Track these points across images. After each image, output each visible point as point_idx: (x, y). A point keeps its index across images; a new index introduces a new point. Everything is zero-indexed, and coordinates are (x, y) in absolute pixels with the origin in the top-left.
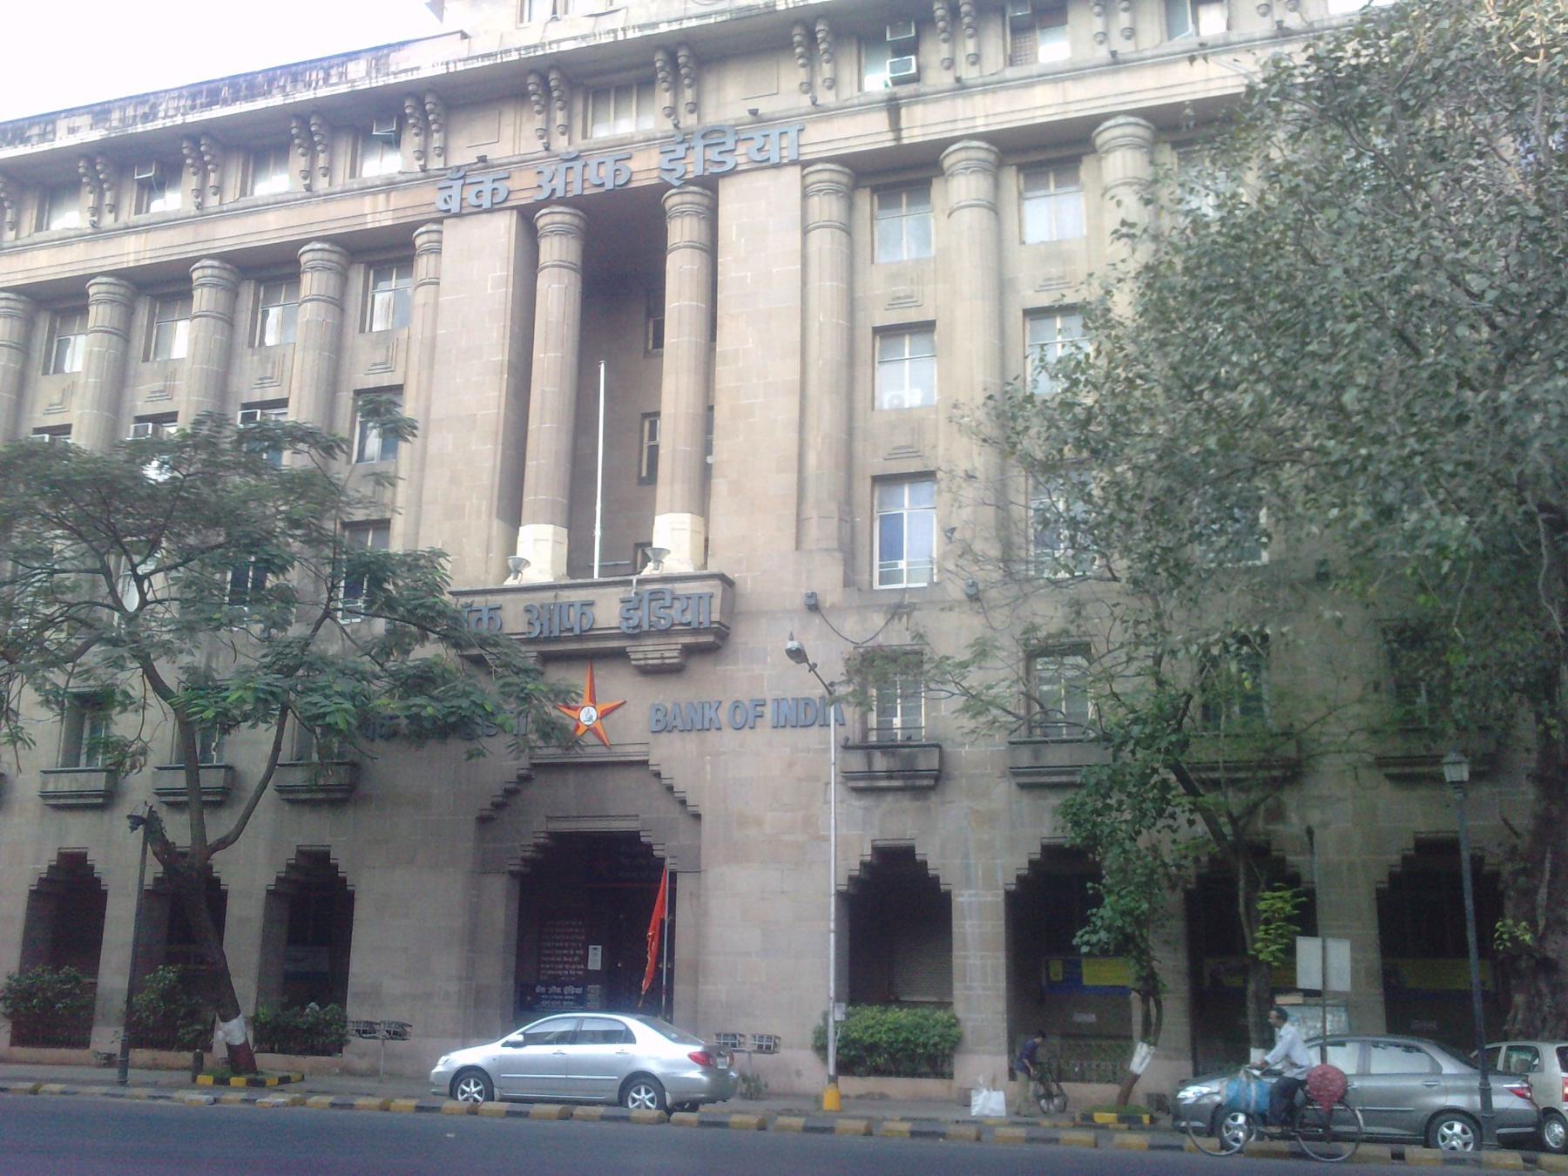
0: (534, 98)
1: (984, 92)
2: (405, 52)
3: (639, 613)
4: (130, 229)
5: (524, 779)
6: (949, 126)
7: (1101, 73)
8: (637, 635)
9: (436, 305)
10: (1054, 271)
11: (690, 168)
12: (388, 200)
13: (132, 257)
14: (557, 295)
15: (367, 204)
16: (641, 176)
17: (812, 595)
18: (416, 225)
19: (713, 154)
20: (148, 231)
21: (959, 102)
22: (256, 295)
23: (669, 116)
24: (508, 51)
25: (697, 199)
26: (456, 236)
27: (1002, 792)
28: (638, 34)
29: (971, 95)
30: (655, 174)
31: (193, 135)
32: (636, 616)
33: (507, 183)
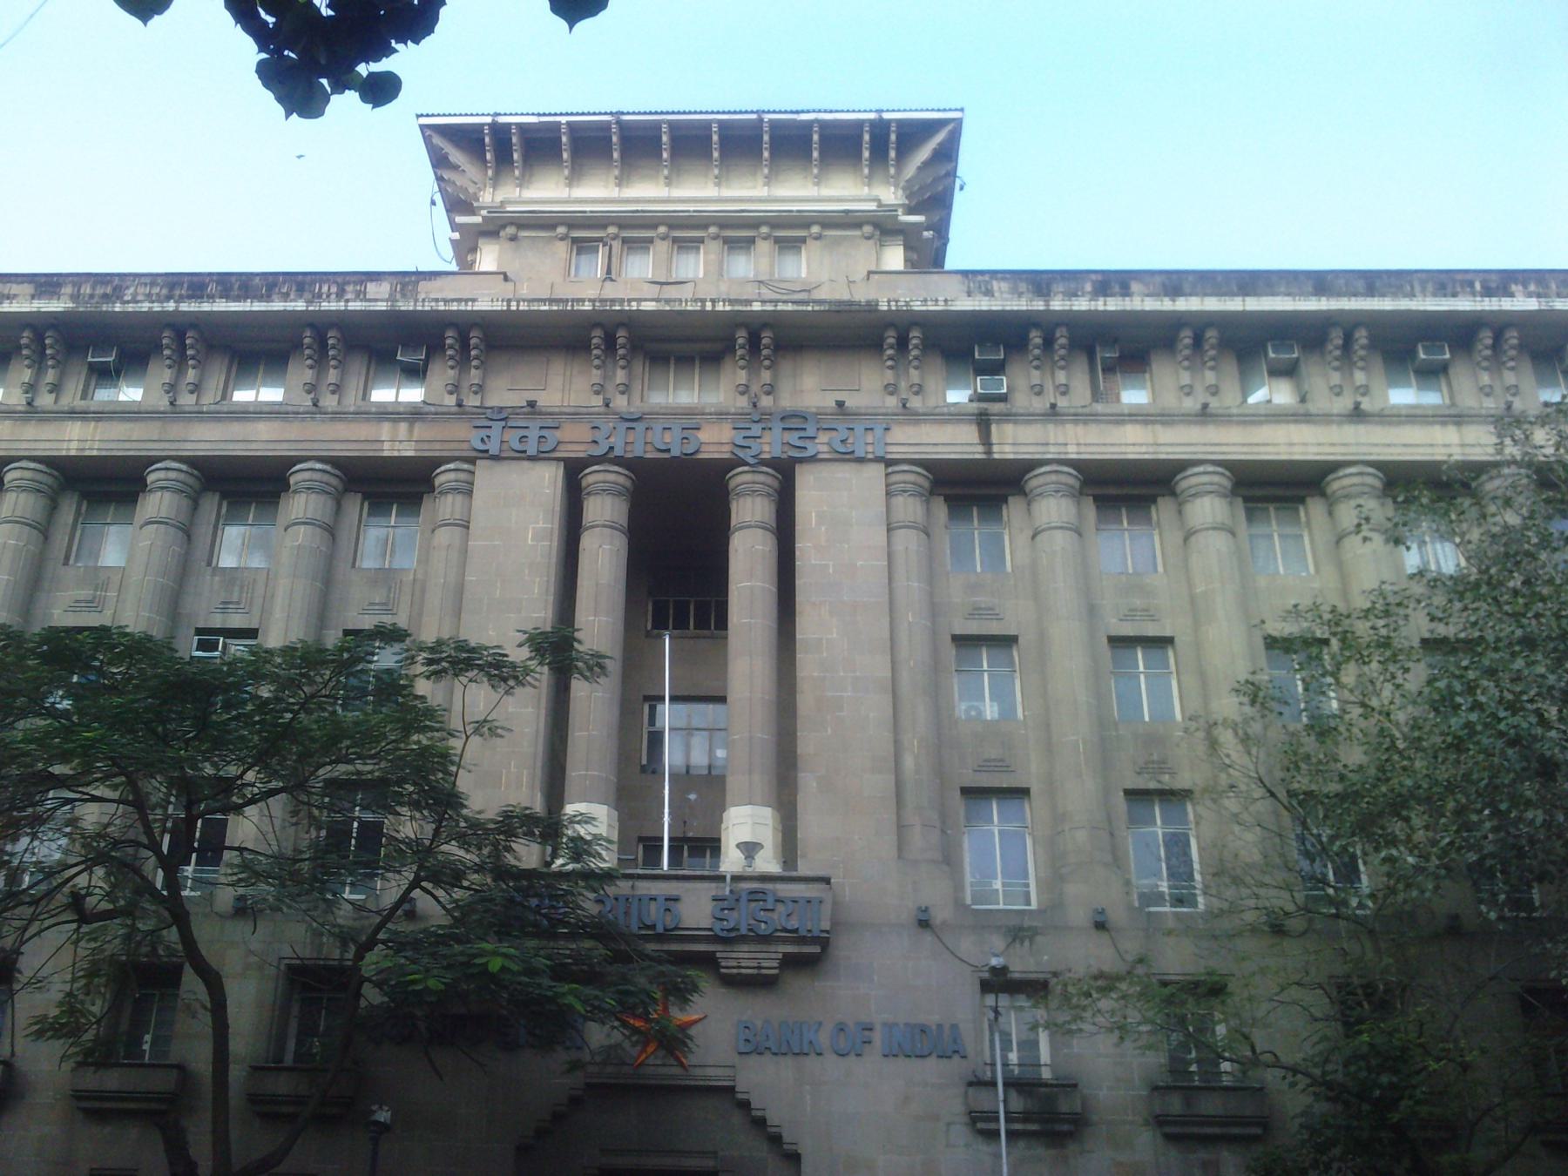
0: (450, 352)
1: (1076, 422)
2: (439, 282)
3: (735, 914)
4: (73, 414)
5: (575, 1101)
6: (1041, 449)
7: (1190, 423)
8: (731, 939)
9: (464, 551)
10: (1138, 602)
11: (766, 448)
12: (411, 431)
13: (74, 445)
14: (604, 557)
15: (385, 431)
16: (711, 448)
18: (437, 462)
19: (793, 438)
20: (99, 420)
21: (1051, 427)
22: (78, 513)
23: (309, 392)
24: (583, 300)
25: (769, 480)
26: (488, 478)
27: (1146, 1145)
28: (728, 308)
29: (1063, 422)
30: (727, 448)
31: (180, 327)
32: (733, 918)
33: (558, 434)
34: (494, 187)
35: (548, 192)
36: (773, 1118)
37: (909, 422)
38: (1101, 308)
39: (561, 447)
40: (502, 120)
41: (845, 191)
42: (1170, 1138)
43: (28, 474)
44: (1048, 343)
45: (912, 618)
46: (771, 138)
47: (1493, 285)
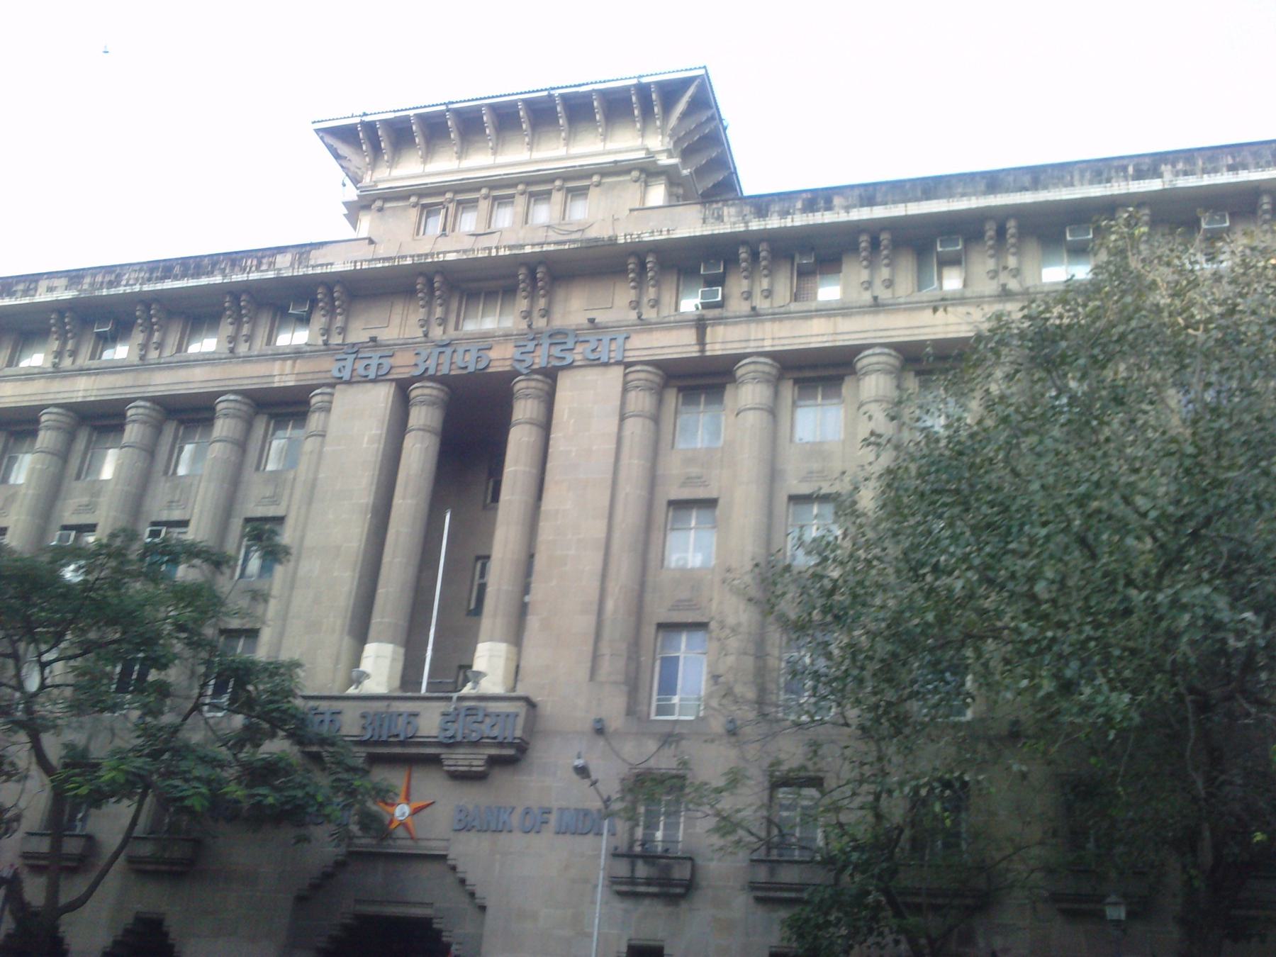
1: (773, 320)
2: (323, 251)
3: (455, 725)
4: (82, 371)
6: (744, 345)
7: (865, 313)
8: (452, 744)
9: (320, 453)
12: (293, 366)
13: (81, 394)
14: (418, 453)
15: (276, 367)
17: (599, 721)
18: (313, 388)
19: (556, 351)
20: (97, 374)
21: (753, 326)
23: (422, 326)
26: (345, 399)
27: (741, 903)
28: (508, 253)
29: (763, 321)
31: (147, 301)
32: (452, 729)
33: (391, 361)
34: (373, 170)
35: (411, 170)
36: (470, 879)
37: (644, 331)
38: (789, 224)
39: (393, 371)
40: (644, 80)
41: (628, 144)
42: (760, 900)
43: (53, 417)
44: (755, 256)
45: (631, 490)
46: (638, 99)
47: (1145, 167)
